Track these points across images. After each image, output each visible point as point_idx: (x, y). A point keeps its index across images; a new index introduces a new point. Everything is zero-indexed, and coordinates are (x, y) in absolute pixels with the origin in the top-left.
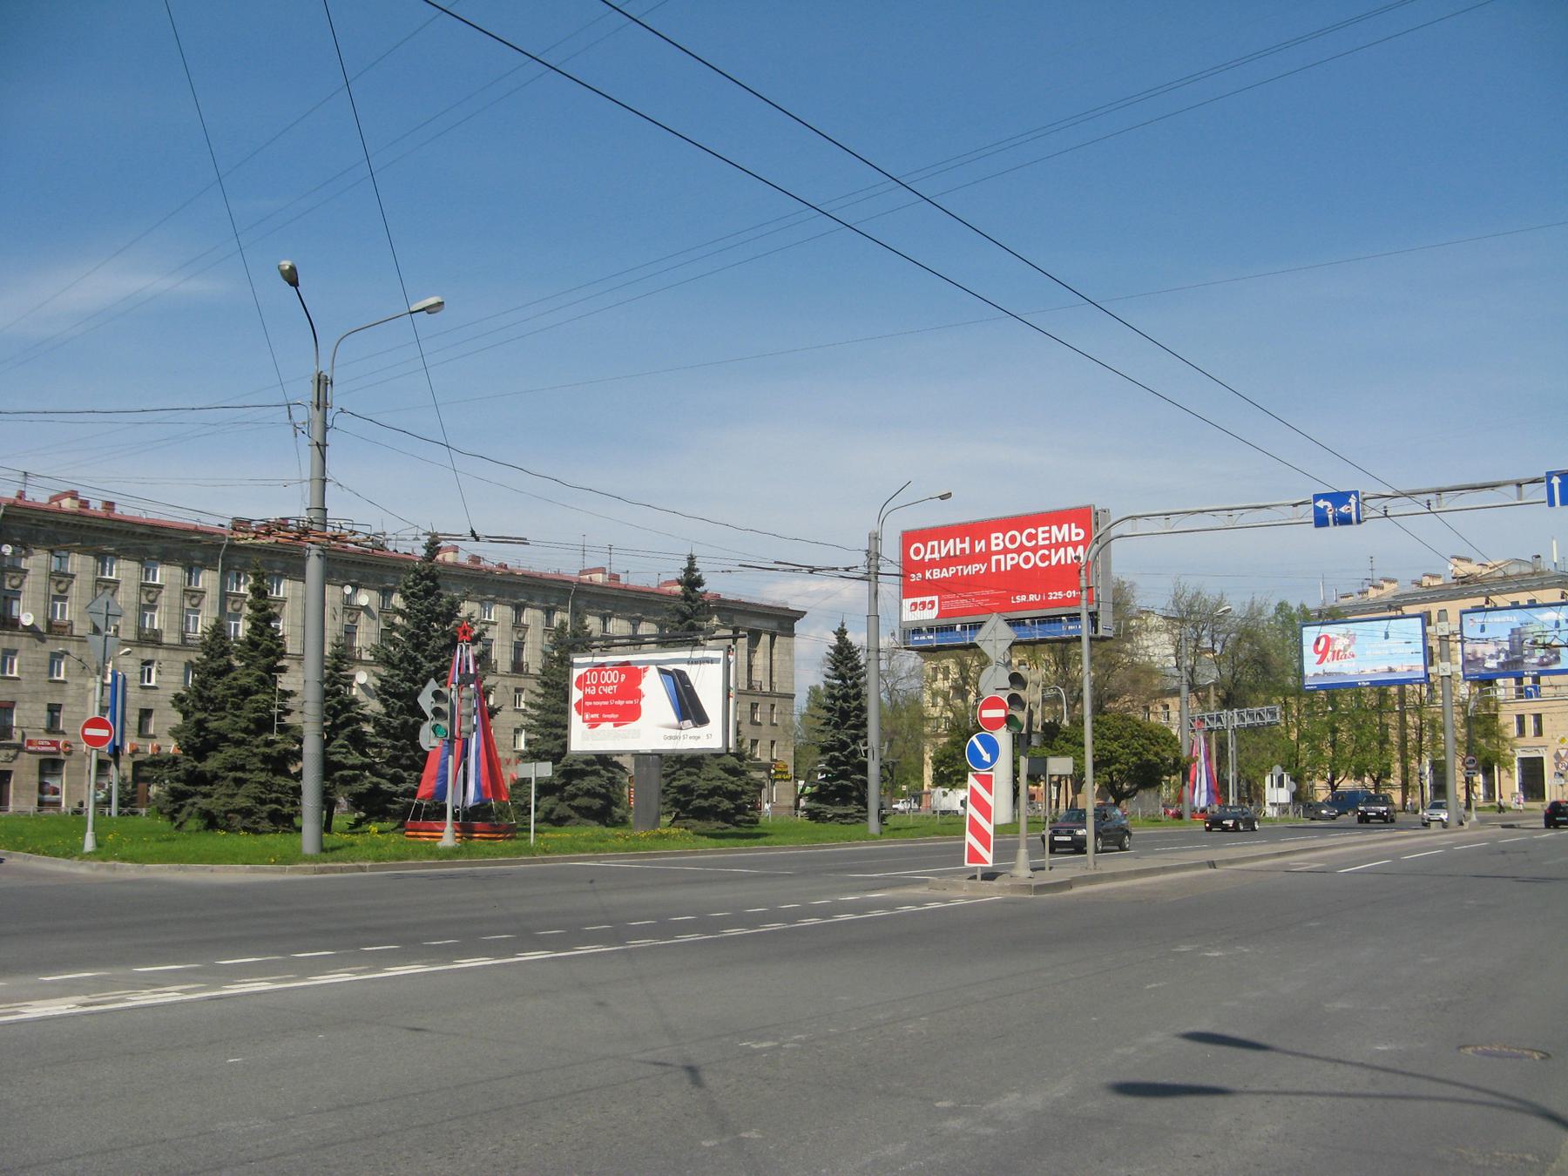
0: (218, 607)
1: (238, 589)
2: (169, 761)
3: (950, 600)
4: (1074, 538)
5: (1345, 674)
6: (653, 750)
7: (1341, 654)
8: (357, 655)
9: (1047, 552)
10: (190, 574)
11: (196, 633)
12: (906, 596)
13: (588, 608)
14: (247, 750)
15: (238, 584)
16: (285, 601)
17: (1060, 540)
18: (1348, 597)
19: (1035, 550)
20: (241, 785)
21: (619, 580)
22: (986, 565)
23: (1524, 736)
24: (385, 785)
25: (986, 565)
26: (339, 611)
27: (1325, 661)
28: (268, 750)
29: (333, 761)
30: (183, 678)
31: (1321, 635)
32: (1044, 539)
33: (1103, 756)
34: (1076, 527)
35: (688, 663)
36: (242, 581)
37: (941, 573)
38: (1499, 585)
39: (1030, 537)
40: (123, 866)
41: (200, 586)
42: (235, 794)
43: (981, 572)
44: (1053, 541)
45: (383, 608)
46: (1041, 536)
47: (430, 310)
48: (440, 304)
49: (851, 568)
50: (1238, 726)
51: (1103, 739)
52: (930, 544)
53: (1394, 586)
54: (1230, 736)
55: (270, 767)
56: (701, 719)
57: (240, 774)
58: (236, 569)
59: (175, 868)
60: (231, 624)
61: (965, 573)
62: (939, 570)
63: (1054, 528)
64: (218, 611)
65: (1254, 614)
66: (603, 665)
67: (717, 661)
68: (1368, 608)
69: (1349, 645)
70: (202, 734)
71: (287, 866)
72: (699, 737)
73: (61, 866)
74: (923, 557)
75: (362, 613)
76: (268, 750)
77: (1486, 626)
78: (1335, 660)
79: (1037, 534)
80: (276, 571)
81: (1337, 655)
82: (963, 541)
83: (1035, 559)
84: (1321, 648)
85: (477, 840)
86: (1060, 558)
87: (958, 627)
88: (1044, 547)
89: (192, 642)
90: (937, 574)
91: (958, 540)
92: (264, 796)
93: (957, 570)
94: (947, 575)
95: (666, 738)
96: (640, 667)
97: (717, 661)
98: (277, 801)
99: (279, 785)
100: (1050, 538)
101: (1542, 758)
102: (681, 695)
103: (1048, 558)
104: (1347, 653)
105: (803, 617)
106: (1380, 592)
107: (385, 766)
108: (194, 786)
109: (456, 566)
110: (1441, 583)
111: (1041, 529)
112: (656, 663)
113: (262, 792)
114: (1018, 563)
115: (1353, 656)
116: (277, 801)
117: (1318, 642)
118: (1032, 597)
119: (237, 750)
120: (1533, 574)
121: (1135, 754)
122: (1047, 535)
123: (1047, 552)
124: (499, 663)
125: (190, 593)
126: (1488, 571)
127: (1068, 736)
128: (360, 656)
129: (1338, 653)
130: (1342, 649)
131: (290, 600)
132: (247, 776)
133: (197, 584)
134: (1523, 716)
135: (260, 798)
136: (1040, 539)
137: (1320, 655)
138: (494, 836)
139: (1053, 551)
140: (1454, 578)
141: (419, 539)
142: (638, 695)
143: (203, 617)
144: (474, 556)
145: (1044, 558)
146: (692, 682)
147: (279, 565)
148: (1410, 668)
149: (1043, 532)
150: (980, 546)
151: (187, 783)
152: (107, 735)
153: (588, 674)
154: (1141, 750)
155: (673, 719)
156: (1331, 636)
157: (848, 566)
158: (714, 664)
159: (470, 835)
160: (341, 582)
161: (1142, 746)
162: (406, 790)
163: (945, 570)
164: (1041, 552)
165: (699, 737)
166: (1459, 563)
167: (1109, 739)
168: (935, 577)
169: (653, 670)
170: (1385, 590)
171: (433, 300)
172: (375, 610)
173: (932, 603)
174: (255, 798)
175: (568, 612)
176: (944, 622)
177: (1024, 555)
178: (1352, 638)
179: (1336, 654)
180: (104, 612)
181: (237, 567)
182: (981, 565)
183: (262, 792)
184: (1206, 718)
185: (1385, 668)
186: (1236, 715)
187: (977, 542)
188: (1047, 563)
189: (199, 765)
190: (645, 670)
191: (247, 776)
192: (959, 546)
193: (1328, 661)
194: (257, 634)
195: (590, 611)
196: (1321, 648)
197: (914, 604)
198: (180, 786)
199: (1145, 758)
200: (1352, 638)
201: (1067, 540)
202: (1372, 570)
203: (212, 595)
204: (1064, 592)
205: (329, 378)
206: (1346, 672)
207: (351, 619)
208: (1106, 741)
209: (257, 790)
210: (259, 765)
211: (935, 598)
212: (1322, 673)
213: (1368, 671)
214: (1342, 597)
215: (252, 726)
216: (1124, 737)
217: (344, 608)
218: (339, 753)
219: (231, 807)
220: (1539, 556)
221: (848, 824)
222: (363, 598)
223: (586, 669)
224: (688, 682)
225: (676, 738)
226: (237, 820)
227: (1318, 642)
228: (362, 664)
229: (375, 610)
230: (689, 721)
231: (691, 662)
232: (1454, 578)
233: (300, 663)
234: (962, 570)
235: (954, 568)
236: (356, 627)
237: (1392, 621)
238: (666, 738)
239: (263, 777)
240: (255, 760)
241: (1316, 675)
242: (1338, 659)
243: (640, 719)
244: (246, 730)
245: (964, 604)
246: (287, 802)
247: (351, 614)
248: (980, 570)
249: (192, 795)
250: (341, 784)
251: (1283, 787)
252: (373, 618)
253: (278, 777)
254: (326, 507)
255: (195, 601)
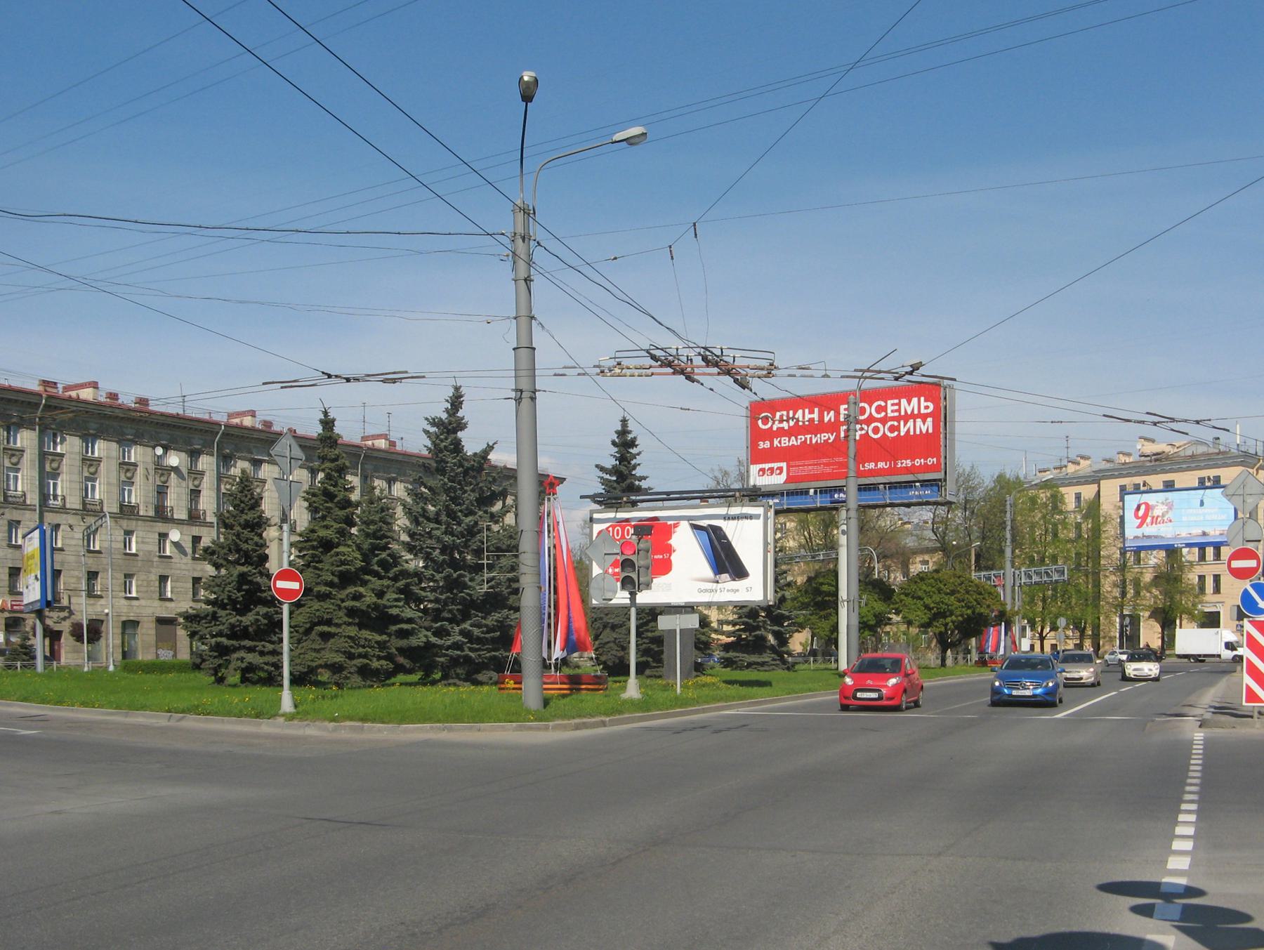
0: (37, 466)
1: (55, 448)
2: (207, 615)
3: (800, 466)
4: (923, 411)
5: (1162, 537)
6: (686, 603)
7: (1159, 519)
8: (169, 514)
9: (896, 423)
10: (9, 433)
11: (16, 491)
12: (754, 462)
13: (375, 472)
14: (333, 604)
15: (55, 443)
16: (101, 461)
17: (909, 412)
18: (1045, 471)
19: (884, 421)
20: (329, 640)
21: (395, 446)
22: (835, 434)
23: (1219, 593)
24: (433, 639)
25: (835, 434)
26: (152, 472)
27: (1145, 525)
28: (357, 604)
29: (392, 615)
30: (7, 535)
31: (1141, 502)
32: (892, 411)
33: (940, 608)
34: (926, 401)
35: (725, 519)
36: (58, 440)
37: (789, 441)
38: (1189, 463)
39: (879, 410)
40: (374, 727)
41: (19, 445)
42: (323, 649)
43: (830, 441)
44: (903, 413)
45: (191, 470)
46: (890, 408)
47: (632, 141)
48: (644, 134)
49: (1201, 421)
50: (1024, 583)
51: (940, 593)
52: (778, 414)
53: (1088, 462)
54: (1017, 591)
55: (357, 621)
56: (739, 572)
57: (326, 629)
58: (53, 429)
59: (439, 728)
60: (49, 483)
61: (814, 441)
62: (787, 439)
63: (904, 402)
64: (37, 470)
65: (1005, 485)
66: (627, 520)
67: (757, 517)
68: (1075, 481)
69: (1167, 512)
70: (244, 587)
71: (551, 723)
72: (738, 590)
73: (265, 727)
74: (772, 426)
75: (172, 473)
76: (357, 604)
77: (1204, 501)
78: (1154, 525)
79: (886, 406)
80: (91, 432)
81: (1155, 520)
82: (811, 412)
83: (884, 430)
84: (1141, 513)
85: (584, 692)
86: (905, 426)
87: (812, 491)
88: (893, 419)
89: (14, 499)
90: (785, 442)
91: (807, 411)
92: (353, 651)
93: (806, 439)
94: (795, 443)
95: (701, 591)
96: (669, 523)
97: (757, 517)
98: (365, 656)
99: (366, 639)
100: (899, 410)
101: (1219, 612)
102: (717, 551)
103: (898, 428)
104: (1165, 519)
105: (562, 483)
106: (1077, 468)
107: (714, 625)
108: (237, 641)
109: (253, 429)
110: (1131, 460)
111: (890, 402)
112: (688, 518)
113: (351, 647)
114: (867, 433)
115: (1170, 521)
116: (365, 656)
117: (1138, 508)
118: (881, 465)
119: (322, 603)
120: (1218, 454)
121: (969, 608)
122: (896, 407)
123: (896, 423)
124: (298, 523)
125: (10, 452)
126: (1176, 450)
127: (906, 591)
128: (172, 515)
129: (1157, 519)
130: (1161, 514)
131: (104, 460)
132: (333, 630)
133: (15, 443)
134: (1204, 576)
135: (350, 653)
136: (889, 411)
137: (1140, 521)
138: (596, 687)
139: (902, 423)
140: (1141, 456)
141: (828, 377)
142: (669, 550)
143: (23, 476)
144: (265, 422)
145: (892, 429)
146: (730, 538)
147: (93, 425)
148: (1222, 532)
149: (893, 405)
150: (829, 417)
151: (229, 637)
152: (298, 588)
153: (611, 529)
154: (975, 603)
155: (709, 573)
156: (1150, 503)
157: (1199, 419)
158: (753, 520)
159: (577, 686)
160: (152, 443)
161: (976, 600)
162: (454, 643)
163: (793, 438)
164: (890, 423)
165: (738, 590)
166: (1146, 443)
167: (947, 594)
168: (783, 445)
169: (684, 525)
170: (1081, 466)
171: (635, 131)
172: (184, 471)
173: (781, 469)
174: (345, 653)
175: (358, 476)
176: (792, 486)
177: (873, 425)
178: (1170, 506)
179: (1155, 519)
180: (288, 455)
181: (53, 426)
182: (830, 434)
183: (351, 647)
184: (993, 577)
185: (1200, 532)
186: (1023, 573)
187: (826, 413)
188: (896, 433)
189: (243, 619)
190: (676, 526)
191: (333, 630)
192: (808, 416)
193: (1147, 525)
194: (332, 485)
195: (377, 475)
196: (1141, 513)
197: (763, 470)
198: (224, 640)
199: (977, 611)
200: (1170, 506)
201: (916, 412)
202: (1067, 448)
203: (31, 454)
204: (926, 459)
205: (531, 208)
206: (1163, 535)
207: (163, 479)
208: (943, 595)
209: (347, 645)
210: (346, 619)
211: (784, 465)
212: (1141, 536)
213: (1184, 535)
214: (1039, 472)
215: (336, 580)
216: (959, 592)
217: (155, 469)
218: (396, 606)
219: (321, 662)
220: (1218, 438)
221: (766, 671)
222: (174, 459)
223: (608, 525)
224: (725, 537)
225: (712, 591)
226: (324, 676)
227: (1138, 508)
228: (175, 523)
229: (184, 471)
230: (727, 575)
231: (727, 518)
232: (1141, 456)
233: (116, 521)
234: (811, 439)
235: (803, 437)
236: (167, 487)
237: (1207, 490)
238: (701, 591)
239: (352, 631)
240: (341, 614)
241: (1136, 537)
242: (1156, 524)
243: (672, 571)
244: (331, 584)
245: (819, 470)
246: (374, 656)
247: (162, 475)
248: (829, 438)
249: (236, 649)
250: (397, 637)
251: (1026, 637)
252: (183, 478)
253: (363, 632)
254: (534, 346)
255: (14, 460)
